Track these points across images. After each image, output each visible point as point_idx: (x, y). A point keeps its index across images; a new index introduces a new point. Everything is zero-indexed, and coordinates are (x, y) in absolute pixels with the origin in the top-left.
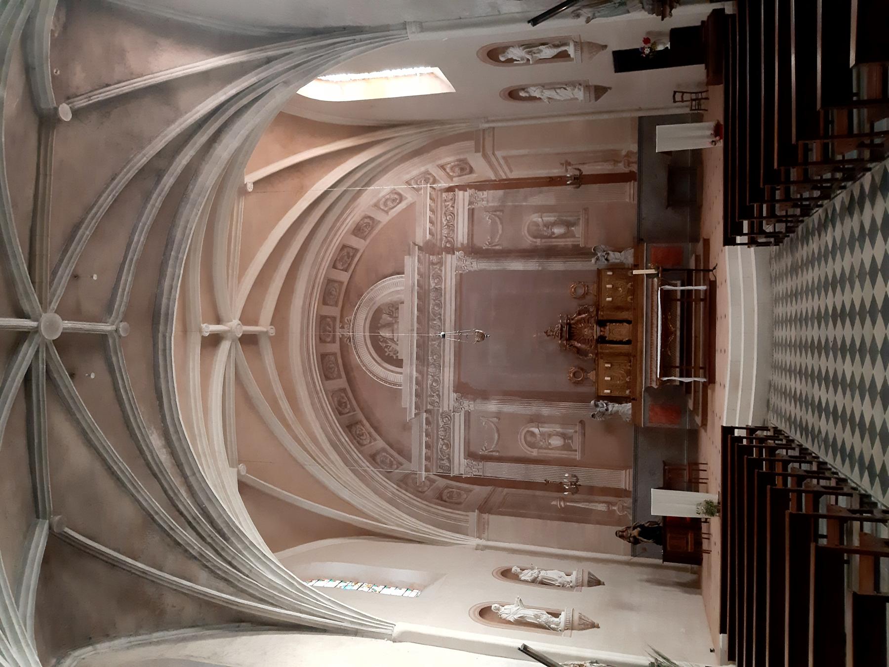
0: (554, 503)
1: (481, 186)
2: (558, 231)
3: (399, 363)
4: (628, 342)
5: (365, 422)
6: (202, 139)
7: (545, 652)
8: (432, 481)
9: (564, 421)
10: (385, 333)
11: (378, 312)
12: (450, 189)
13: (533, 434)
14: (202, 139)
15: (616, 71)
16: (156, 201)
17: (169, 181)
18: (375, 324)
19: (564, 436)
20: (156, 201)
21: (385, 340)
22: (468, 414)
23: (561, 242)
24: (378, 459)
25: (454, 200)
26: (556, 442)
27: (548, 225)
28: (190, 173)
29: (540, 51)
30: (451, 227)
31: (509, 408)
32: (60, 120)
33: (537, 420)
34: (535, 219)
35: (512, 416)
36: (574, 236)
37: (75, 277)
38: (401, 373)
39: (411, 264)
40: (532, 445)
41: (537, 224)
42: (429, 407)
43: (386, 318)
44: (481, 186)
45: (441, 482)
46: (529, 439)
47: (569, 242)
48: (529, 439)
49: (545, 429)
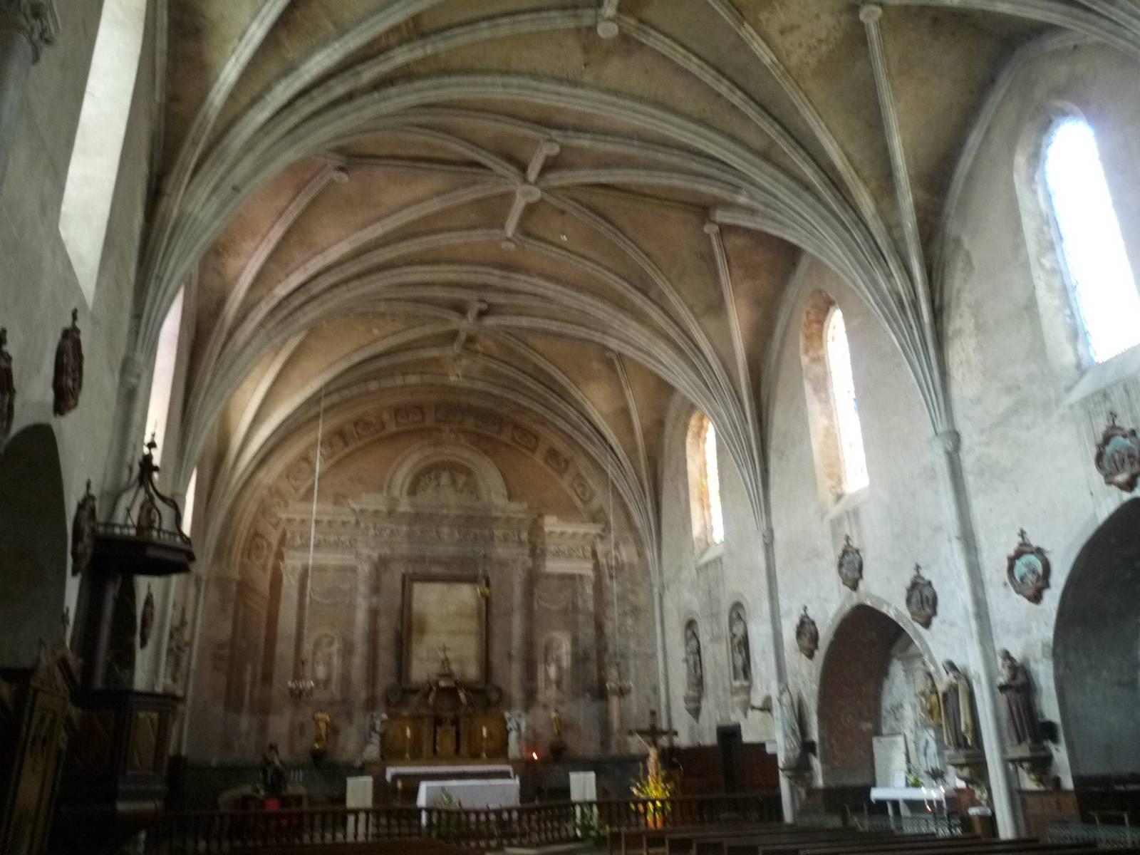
0: (249, 667)
1: (599, 587)
2: (552, 671)
3: (413, 490)
4: (435, 751)
5: (347, 450)
6: (673, 332)
7: (806, 706)
8: (276, 526)
9: (346, 680)
10: (445, 478)
11: (469, 473)
12: (594, 554)
13: (331, 644)
14: (673, 332)
15: (739, 726)
16: (621, 286)
17: (637, 299)
18: (455, 468)
19: (327, 682)
20: (621, 286)
21: (438, 478)
22: (354, 570)
23: (541, 676)
24: (304, 465)
25: (585, 557)
26: (321, 672)
27: (558, 661)
28: (641, 318)
29: (740, 653)
30: (558, 554)
31: (361, 617)
32: (704, 223)
33: (347, 651)
34: (564, 645)
35: (350, 623)
36: (546, 688)
37: (563, 212)
38: (401, 493)
39: (517, 509)
40: (317, 644)
41: (559, 647)
42: (362, 525)
43: (461, 480)
44: (599, 587)
45: (274, 538)
46: (325, 640)
47: (541, 683)
48: (325, 640)
49: (336, 660)
